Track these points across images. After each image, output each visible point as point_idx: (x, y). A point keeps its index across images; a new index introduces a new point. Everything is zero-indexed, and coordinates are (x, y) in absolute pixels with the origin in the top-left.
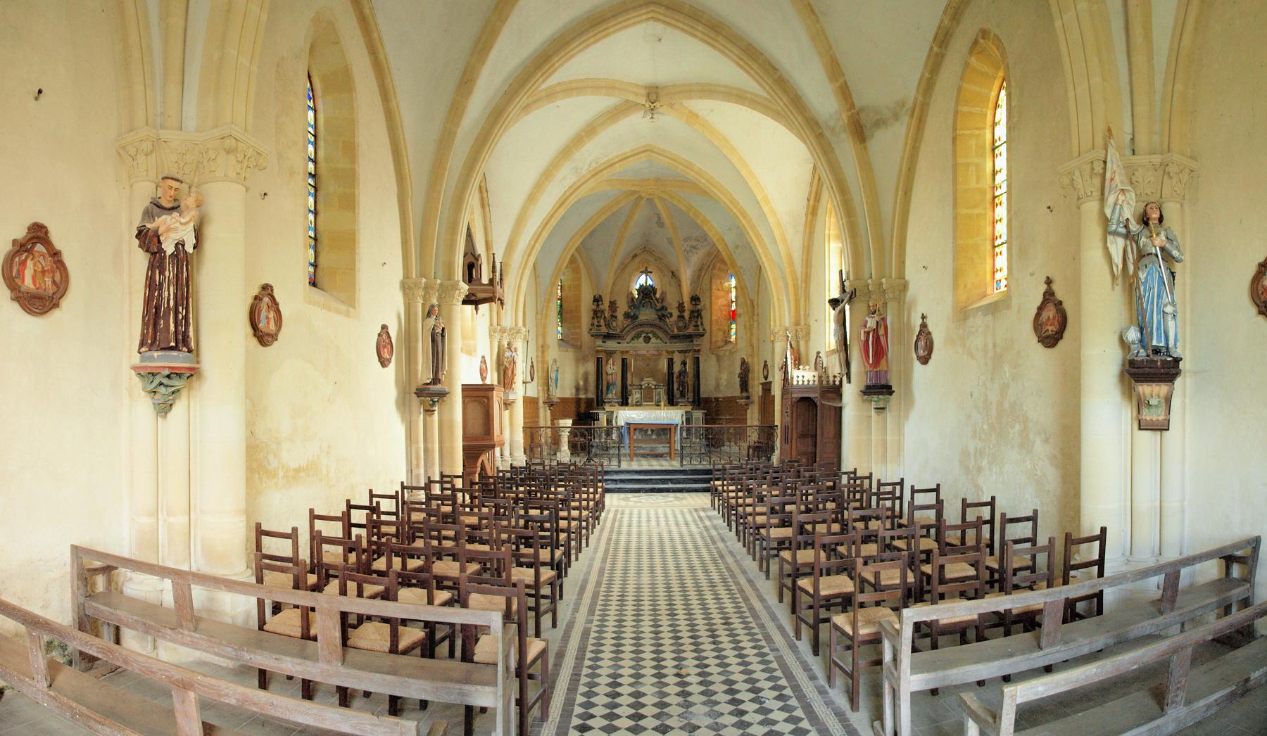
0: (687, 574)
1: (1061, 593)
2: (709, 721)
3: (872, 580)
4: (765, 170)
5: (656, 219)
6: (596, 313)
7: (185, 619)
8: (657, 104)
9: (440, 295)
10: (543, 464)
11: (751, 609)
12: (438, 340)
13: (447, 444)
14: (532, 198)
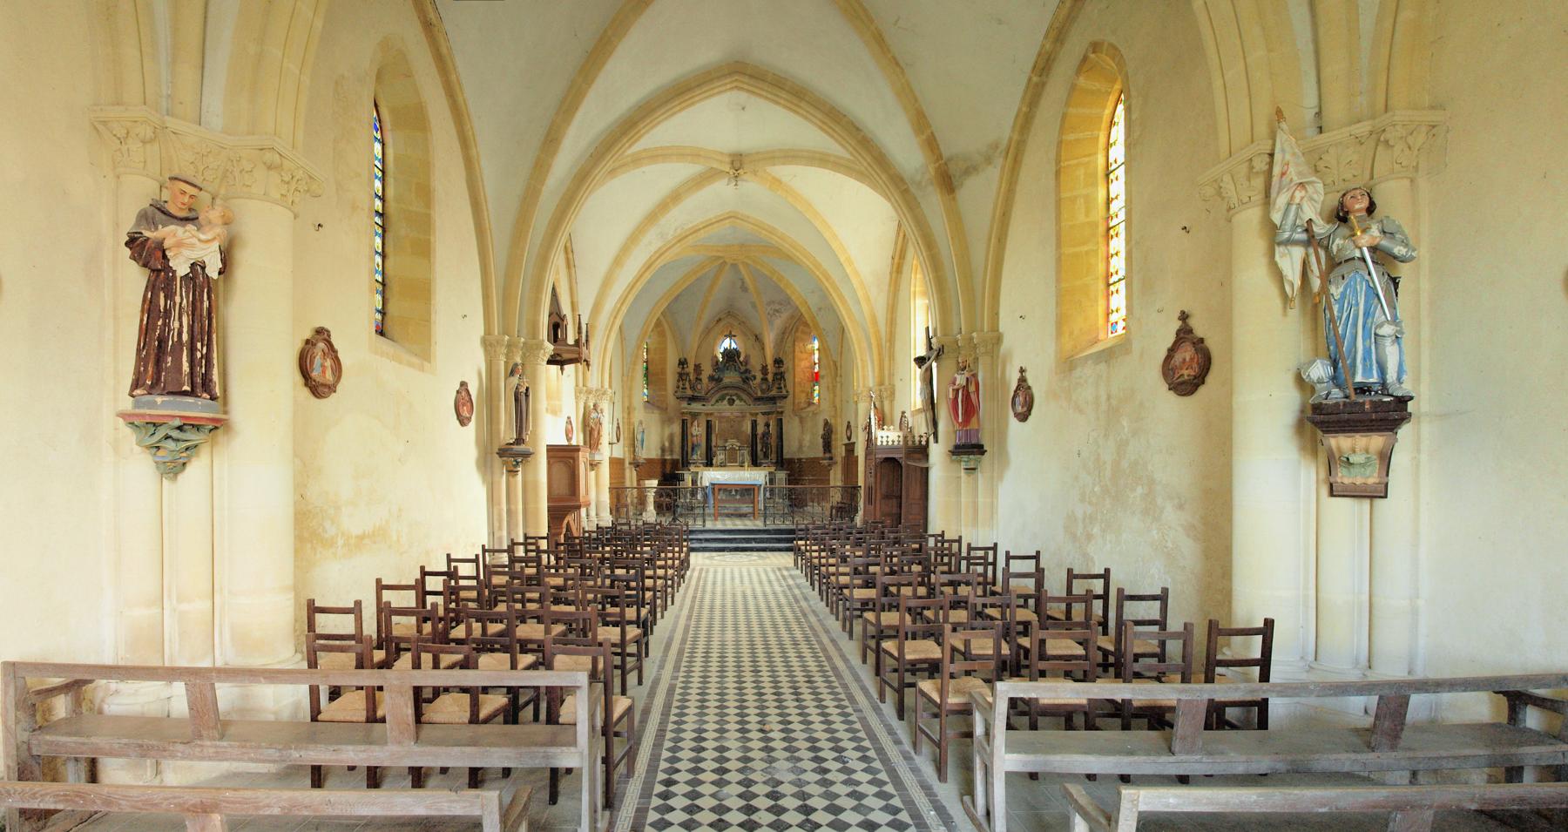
1: (1201, 693)
2: (792, 777)
3: (962, 648)
4: (848, 231)
5: (739, 284)
6: (682, 376)
7: (206, 724)
10: (629, 524)
11: (835, 669)
12: (522, 401)
13: (531, 506)
14: (618, 262)
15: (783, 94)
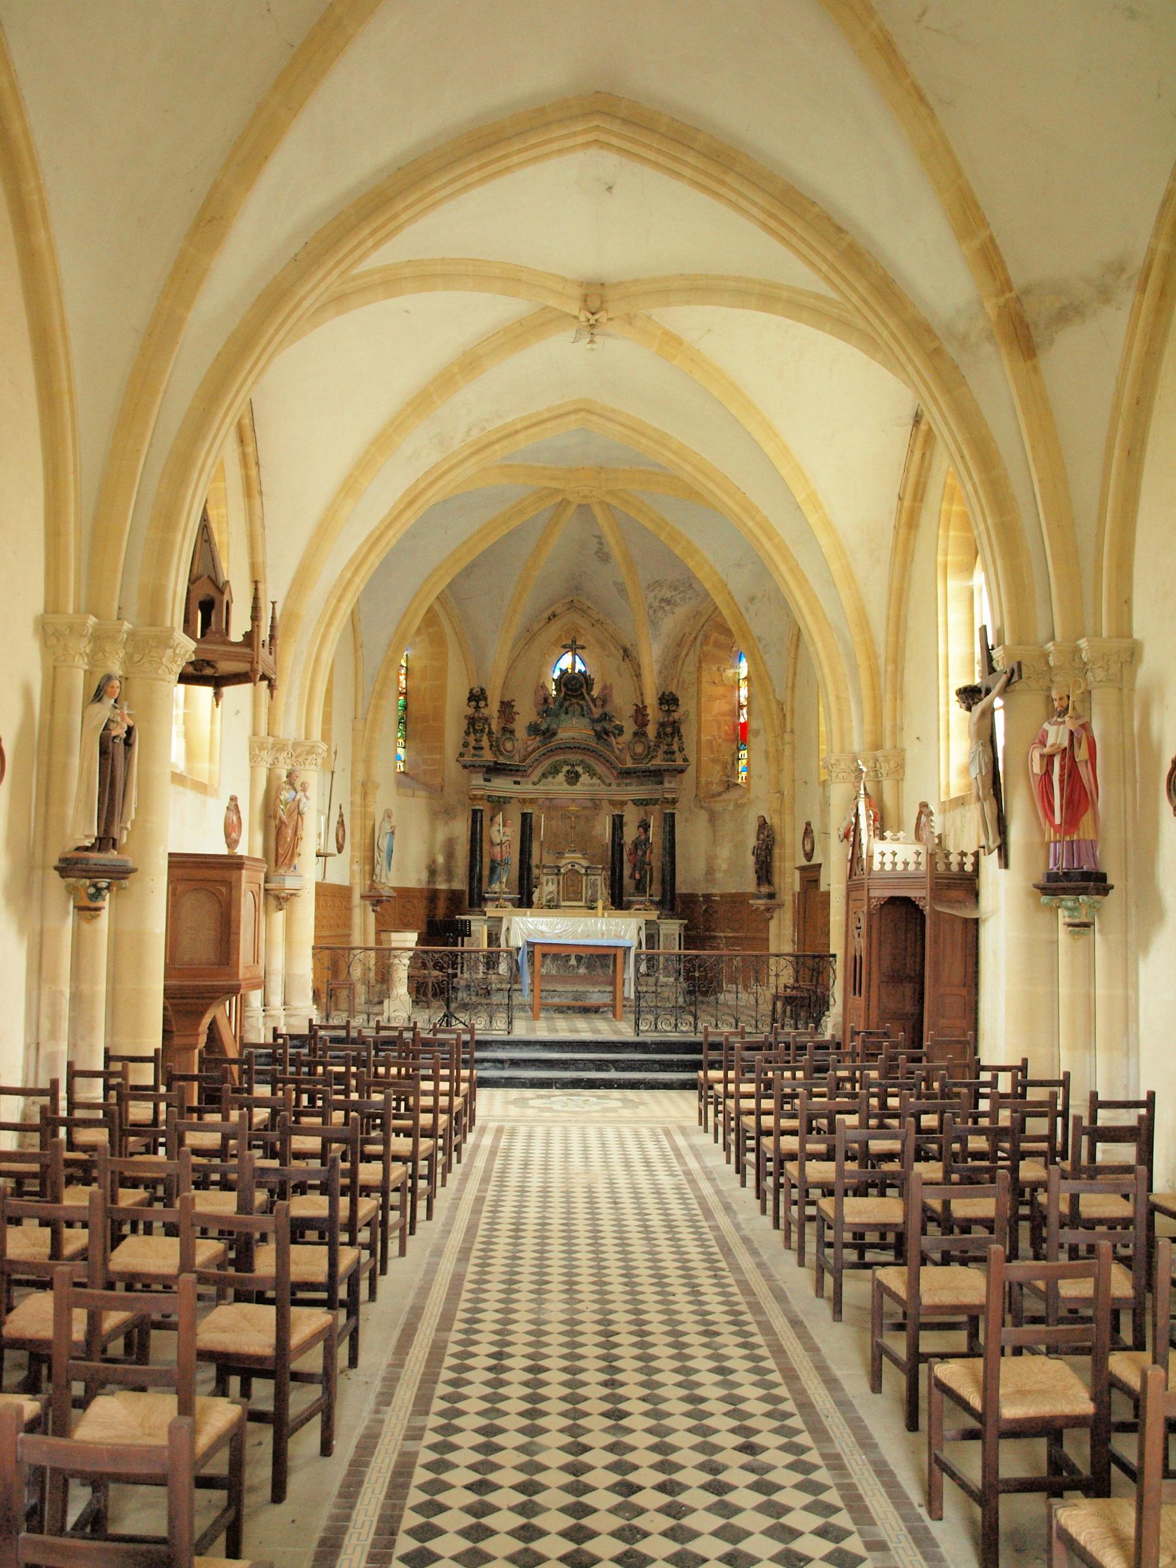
0: (649, 1294)
4: (808, 439)
6: (474, 724)
8: (602, 316)
9: (129, 656)
11: (806, 1406)
12: (116, 754)
15: (690, 158)
